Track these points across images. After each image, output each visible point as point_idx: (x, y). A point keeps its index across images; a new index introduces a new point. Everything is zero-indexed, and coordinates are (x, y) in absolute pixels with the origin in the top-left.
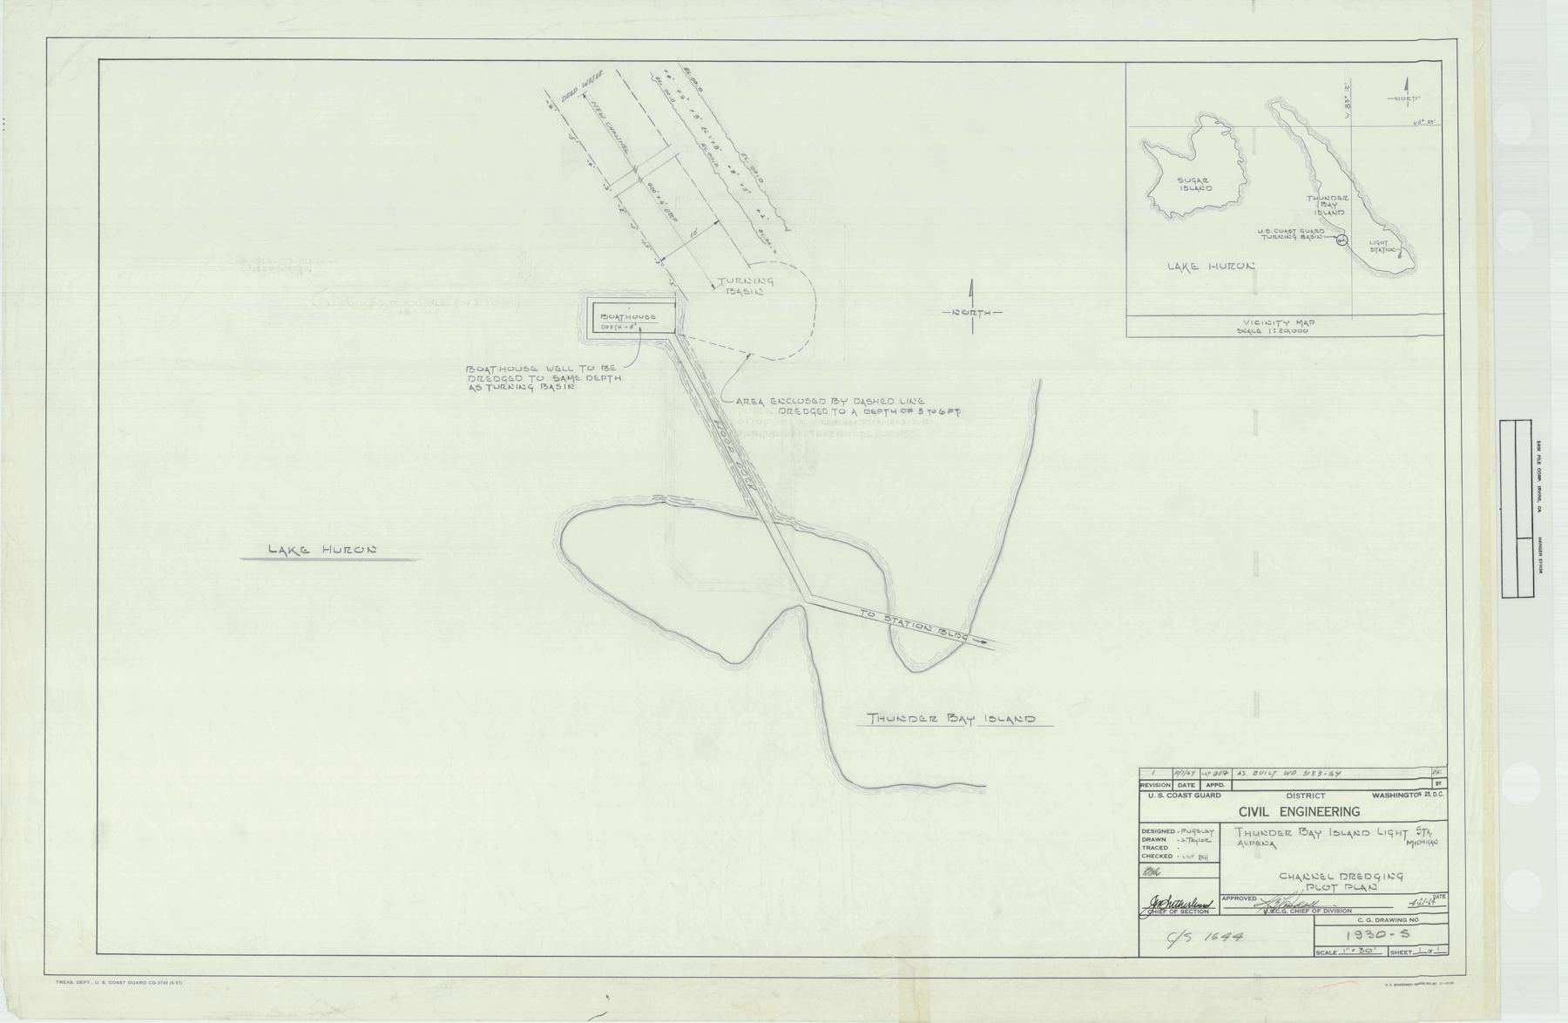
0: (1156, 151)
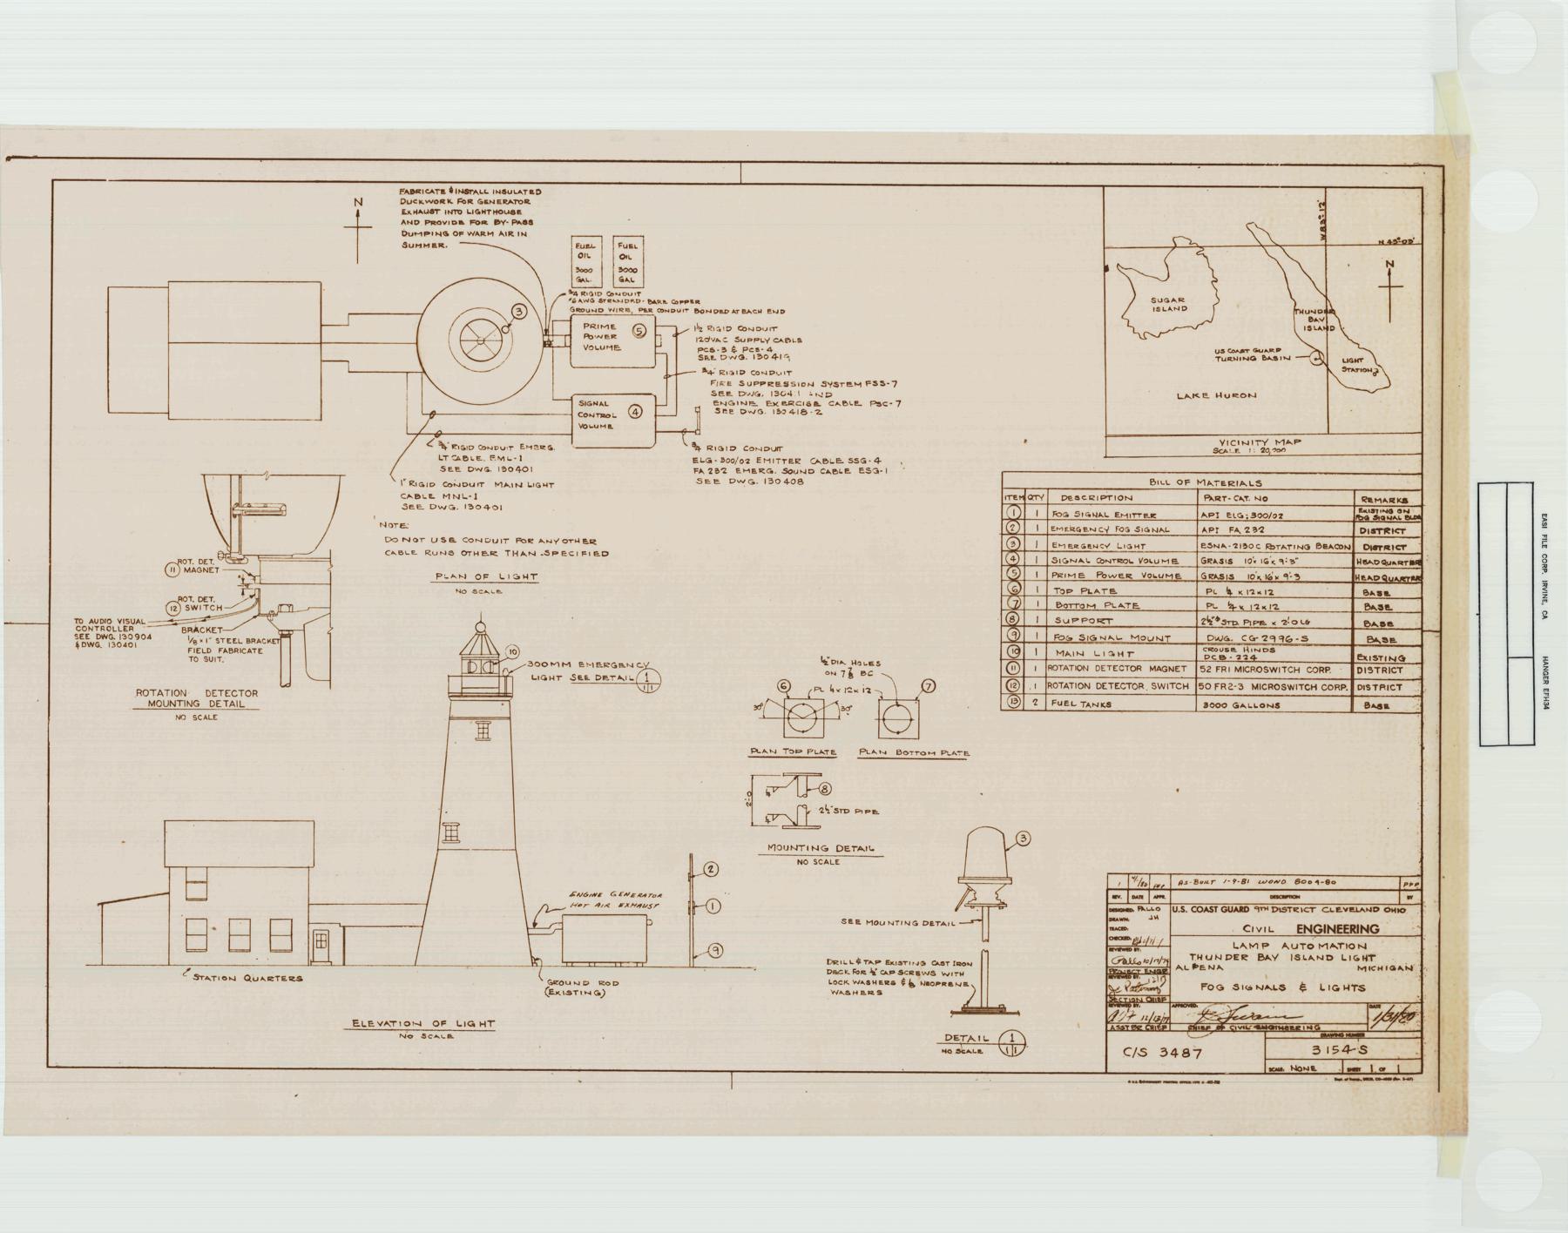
0: (1131, 274)
